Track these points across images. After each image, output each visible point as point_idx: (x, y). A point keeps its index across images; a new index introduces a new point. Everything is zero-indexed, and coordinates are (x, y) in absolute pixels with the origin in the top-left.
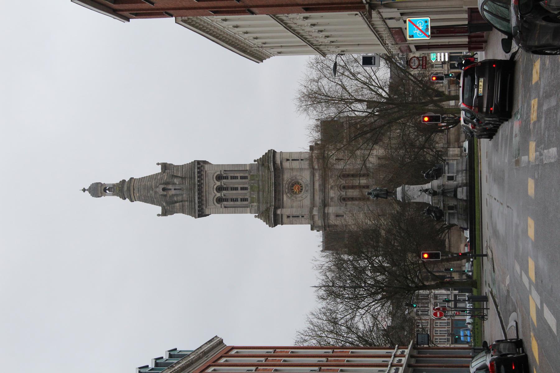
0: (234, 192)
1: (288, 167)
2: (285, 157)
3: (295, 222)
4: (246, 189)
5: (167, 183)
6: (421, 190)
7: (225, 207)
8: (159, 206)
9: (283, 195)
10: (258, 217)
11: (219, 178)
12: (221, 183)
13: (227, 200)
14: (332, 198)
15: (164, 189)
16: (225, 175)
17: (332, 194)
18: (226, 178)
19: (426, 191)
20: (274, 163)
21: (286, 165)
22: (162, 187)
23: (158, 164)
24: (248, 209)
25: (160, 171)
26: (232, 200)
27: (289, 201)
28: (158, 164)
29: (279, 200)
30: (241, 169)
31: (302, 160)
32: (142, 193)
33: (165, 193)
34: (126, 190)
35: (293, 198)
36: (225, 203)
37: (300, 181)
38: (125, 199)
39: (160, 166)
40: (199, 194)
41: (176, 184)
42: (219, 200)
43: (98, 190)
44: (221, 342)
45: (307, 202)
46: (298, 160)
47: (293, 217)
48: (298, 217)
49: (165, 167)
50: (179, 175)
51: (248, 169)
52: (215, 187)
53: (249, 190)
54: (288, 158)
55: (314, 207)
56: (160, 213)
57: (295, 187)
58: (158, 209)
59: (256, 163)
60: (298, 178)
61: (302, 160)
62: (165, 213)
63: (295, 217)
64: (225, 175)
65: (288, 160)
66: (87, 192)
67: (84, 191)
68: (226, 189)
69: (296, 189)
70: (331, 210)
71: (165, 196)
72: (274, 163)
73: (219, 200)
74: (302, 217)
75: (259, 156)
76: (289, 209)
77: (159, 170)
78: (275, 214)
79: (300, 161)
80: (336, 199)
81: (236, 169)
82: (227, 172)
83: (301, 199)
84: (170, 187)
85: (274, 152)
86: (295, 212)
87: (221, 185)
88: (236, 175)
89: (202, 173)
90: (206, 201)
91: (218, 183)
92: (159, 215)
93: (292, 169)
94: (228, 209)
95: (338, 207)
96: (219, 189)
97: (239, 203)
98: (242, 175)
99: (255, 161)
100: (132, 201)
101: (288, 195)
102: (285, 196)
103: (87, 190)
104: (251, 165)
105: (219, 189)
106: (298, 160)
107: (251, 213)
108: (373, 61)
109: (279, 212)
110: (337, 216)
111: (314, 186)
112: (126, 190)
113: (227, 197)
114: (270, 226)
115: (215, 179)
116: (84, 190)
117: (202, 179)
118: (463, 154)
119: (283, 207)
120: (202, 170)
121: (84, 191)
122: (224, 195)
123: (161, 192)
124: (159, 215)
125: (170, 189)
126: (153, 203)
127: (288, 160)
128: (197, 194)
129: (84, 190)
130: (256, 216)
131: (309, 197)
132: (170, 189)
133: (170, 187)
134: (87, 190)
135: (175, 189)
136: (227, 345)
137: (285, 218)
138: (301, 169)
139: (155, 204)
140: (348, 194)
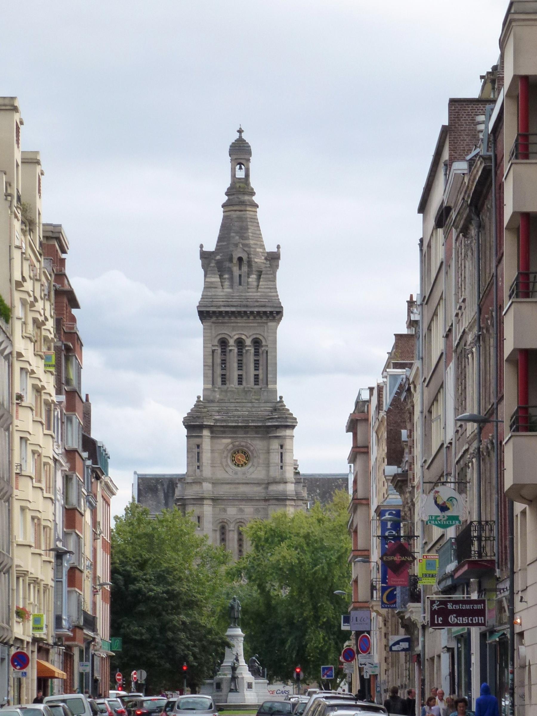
0: (235, 365)
1: (271, 447)
2: (287, 443)
3: (190, 456)
4: (240, 382)
5: (250, 263)
6: (237, 654)
7: (213, 351)
8: (216, 249)
9: (230, 438)
10: (199, 401)
11: (257, 343)
12: (250, 346)
13: (224, 352)
14: (225, 510)
15: (240, 259)
16: (261, 353)
17: (232, 511)
18: (257, 353)
19: (237, 660)
20: (277, 427)
21: (275, 445)
22: (245, 257)
23: (278, 247)
24: (210, 386)
25: (268, 250)
26: (224, 362)
27: (222, 447)
28: (278, 247)
29: (224, 432)
30: (269, 376)
31: (282, 467)
32: (236, 224)
33: (235, 261)
34: (239, 196)
35: (226, 453)
36: (219, 351)
37: (250, 464)
38: (227, 194)
39: (275, 250)
40: (233, 312)
41: (249, 277)
42: (223, 343)
43: (240, 152)
44: (113, 494)
45: (220, 474)
46: (282, 461)
47: (198, 453)
48: (198, 460)
49: (274, 258)
50: (261, 283)
51: (270, 386)
52: (244, 337)
53: (238, 386)
54: (284, 447)
55: (213, 483)
56: (204, 249)
57: (241, 456)
58: (211, 246)
59: (278, 399)
60: (255, 460)
61: (282, 467)
62: (205, 256)
63: (198, 456)
64: (260, 351)
65: (282, 447)
66: (237, 136)
67: (238, 131)
68: (240, 354)
69: (241, 458)
70: (208, 510)
71: (231, 260)
72: (277, 427)
73: (223, 343)
74: (198, 467)
75: (288, 404)
76: (209, 448)
77: (270, 248)
78: (201, 427)
79: (280, 464)
80: (224, 517)
81: (269, 368)
82: (265, 355)
83: (224, 464)
84: (245, 269)
85: (293, 427)
86: (206, 456)
87: (246, 346)
88: (261, 368)
89: (264, 318)
90: (222, 323)
91: (248, 342)
92: (201, 246)
93: (268, 452)
94: (210, 355)
95: (211, 520)
96: (240, 343)
97: (218, 371)
98: (261, 377)
99: (281, 398)
100: (223, 206)
101: (231, 446)
102: (229, 441)
103: (240, 137)
104: (276, 391)
105: (240, 343)
106: (282, 461)
107: (205, 390)
108: (346, 624)
109: (206, 433)
110: (199, 518)
111: (243, 483)
112: (239, 196)
113: (227, 354)
114: (185, 418)
115: (255, 336)
116: (240, 131)
117: (255, 317)
118: (83, 646)
119: (212, 438)
120: (268, 317)
121: (238, 131)
122: (231, 350)
123: (236, 256)
124: (201, 246)
125: (240, 268)
126: (221, 239)
127: (282, 447)
128: (233, 309)
129: (240, 131)
130: (199, 397)
131: (226, 476)
132: (240, 268)
133: (245, 269)
134: (240, 137)
135: (240, 276)
136: (111, 500)
137: (197, 441)
138: (268, 465)
139: (218, 242)
140: (231, 533)
